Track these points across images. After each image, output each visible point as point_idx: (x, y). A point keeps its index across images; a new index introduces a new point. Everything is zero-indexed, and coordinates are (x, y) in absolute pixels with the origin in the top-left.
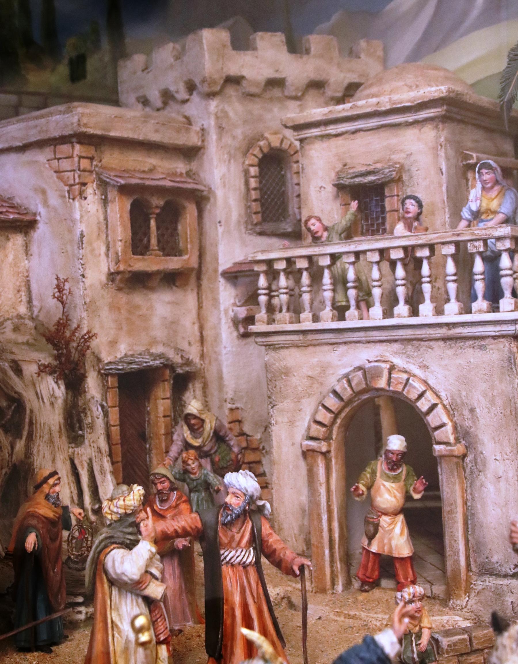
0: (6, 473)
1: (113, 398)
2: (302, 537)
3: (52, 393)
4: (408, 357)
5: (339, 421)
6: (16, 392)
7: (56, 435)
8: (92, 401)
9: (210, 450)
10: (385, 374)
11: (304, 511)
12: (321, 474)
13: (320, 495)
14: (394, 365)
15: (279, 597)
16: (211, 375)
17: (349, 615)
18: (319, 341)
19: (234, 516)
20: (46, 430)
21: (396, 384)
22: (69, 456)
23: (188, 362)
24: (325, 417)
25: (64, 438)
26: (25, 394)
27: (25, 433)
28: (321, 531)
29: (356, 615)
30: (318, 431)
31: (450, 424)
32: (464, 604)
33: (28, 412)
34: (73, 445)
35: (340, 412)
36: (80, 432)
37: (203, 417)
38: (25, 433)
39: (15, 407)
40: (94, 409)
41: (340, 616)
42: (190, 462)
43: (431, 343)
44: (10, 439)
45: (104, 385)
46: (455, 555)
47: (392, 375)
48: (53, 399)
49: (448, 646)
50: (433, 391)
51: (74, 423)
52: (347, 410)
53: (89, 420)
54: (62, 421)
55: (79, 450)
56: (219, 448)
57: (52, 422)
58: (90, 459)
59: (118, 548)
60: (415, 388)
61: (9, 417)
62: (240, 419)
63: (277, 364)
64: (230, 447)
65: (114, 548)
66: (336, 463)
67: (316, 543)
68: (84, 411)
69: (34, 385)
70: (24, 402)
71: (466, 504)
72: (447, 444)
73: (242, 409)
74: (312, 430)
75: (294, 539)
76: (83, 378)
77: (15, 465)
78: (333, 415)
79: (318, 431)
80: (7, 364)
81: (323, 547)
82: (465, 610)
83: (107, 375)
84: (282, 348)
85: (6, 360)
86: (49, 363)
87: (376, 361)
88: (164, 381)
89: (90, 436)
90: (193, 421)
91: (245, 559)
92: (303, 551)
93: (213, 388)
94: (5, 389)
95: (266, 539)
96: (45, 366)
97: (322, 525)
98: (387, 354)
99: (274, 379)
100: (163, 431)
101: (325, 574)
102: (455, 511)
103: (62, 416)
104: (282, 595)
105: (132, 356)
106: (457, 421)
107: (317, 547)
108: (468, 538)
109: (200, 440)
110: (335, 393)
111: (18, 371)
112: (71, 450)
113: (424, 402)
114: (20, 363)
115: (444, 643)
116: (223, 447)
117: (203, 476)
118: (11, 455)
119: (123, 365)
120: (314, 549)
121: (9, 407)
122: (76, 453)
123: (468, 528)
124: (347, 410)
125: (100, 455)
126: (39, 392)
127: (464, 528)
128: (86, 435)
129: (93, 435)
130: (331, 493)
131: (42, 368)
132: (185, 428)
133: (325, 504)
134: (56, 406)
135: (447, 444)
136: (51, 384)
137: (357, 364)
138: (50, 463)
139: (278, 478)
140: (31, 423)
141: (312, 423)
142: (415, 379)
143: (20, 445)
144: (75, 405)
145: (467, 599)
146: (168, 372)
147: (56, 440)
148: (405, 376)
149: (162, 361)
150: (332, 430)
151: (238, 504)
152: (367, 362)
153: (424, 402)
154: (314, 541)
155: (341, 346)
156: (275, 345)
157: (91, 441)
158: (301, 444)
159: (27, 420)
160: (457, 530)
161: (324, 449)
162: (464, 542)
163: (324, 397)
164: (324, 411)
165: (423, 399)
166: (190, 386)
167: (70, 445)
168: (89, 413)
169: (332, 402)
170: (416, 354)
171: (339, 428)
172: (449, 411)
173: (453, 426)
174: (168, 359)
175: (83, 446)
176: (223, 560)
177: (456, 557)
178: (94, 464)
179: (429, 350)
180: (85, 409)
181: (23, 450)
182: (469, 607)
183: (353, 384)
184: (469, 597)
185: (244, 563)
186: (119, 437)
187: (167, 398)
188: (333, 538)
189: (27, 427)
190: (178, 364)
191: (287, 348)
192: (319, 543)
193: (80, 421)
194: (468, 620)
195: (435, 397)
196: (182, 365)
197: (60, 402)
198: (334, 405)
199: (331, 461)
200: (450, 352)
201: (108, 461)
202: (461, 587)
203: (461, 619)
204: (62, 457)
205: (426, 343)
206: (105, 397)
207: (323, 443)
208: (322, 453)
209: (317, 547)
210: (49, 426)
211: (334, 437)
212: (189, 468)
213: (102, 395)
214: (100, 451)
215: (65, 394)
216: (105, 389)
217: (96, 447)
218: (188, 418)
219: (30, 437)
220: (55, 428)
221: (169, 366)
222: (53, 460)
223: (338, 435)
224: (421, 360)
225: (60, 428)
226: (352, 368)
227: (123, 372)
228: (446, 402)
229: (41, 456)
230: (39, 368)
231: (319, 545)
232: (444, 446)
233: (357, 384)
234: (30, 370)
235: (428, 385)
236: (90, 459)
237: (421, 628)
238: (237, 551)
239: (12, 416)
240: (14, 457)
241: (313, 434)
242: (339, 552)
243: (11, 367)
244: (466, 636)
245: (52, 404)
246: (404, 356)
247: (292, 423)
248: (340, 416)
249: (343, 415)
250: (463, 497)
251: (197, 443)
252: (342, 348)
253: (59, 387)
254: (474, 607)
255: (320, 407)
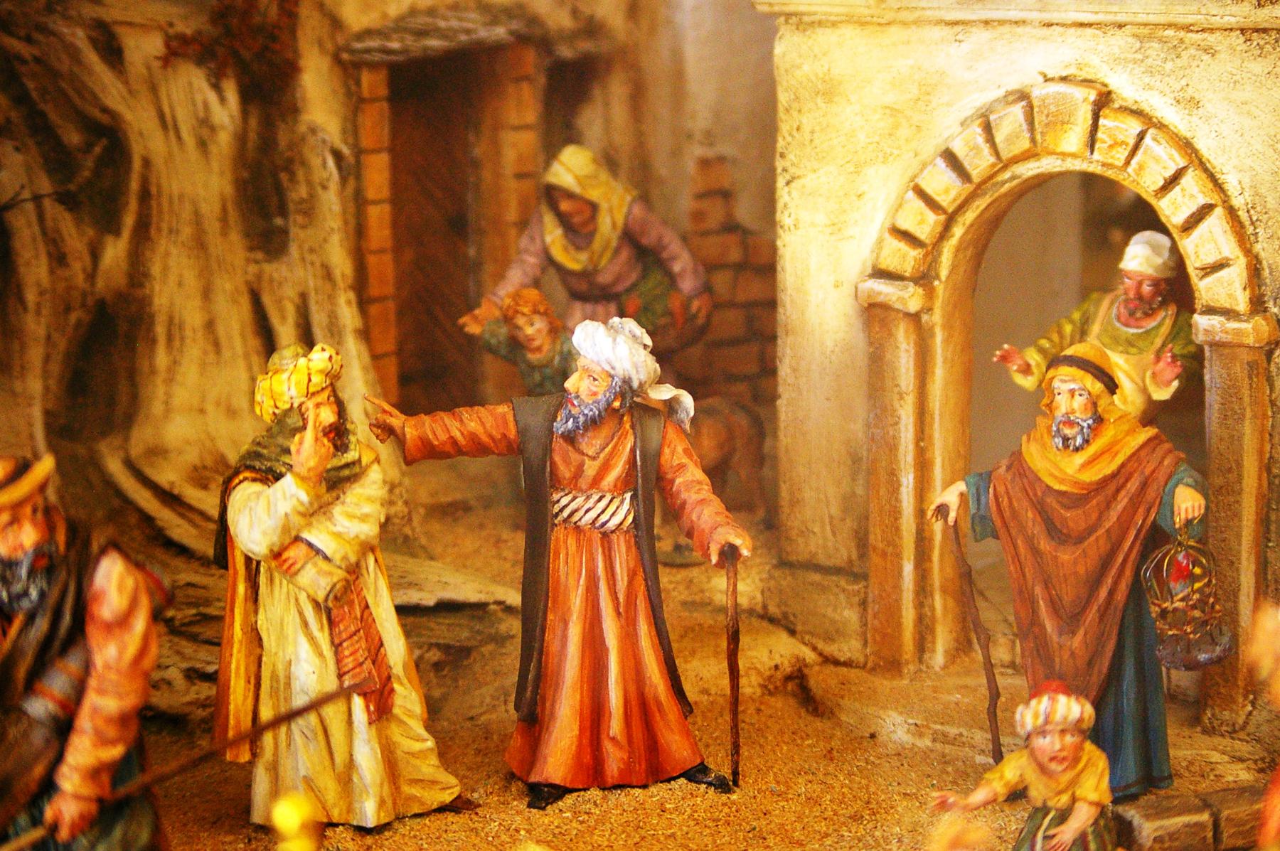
0: (79, 324)
1: (376, 125)
2: (850, 523)
3: (202, 114)
4: (1150, 71)
5: (958, 231)
6: (105, 110)
7: (213, 226)
8: (312, 140)
9: (618, 279)
10: (1084, 116)
11: (856, 460)
12: (903, 370)
13: (897, 423)
14: (1109, 93)
15: (779, 675)
16: (655, 63)
17: (945, 735)
18: (917, 14)
19: (582, 419)
20: (187, 213)
21: (1111, 147)
22: (248, 283)
23: (592, 28)
24: (922, 222)
25: (235, 237)
26: (128, 116)
27: (129, 220)
28: (896, 513)
29: (961, 735)
30: (903, 258)
31: (1242, 261)
32: (1241, 721)
33: (137, 164)
34: (259, 255)
35: (961, 208)
36: (279, 221)
37: (594, 194)
38: (129, 220)
39: (105, 149)
40: (315, 162)
41: (921, 735)
42: (521, 321)
43: (1211, 39)
44: (90, 232)
45: (349, 94)
46: (1228, 600)
47: (1101, 121)
48: (205, 132)
49: (1155, 839)
50: (1206, 170)
51: (265, 201)
52: (981, 203)
53: (303, 191)
54: (229, 190)
55: (275, 270)
56: (643, 277)
57: (202, 193)
58: (304, 296)
59: (254, 480)
60: (1157, 159)
61: (87, 174)
62: (726, 185)
63: (806, 68)
64: (672, 279)
65: (245, 479)
66: (946, 341)
67: (881, 545)
68: (289, 166)
69: (154, 89)
70: (127, 139)
71: (1269, 471)
72: (1229, 313)
73: (734, 161)
74: (886, 252)
75: (828, 528)
76: (288, 71)
77: (101, 304)
78: (942, 218)
79: (903, 258)
80: (80, 33)
81: (899, 556)
82: (1242, 735)
83: (358, 66)
84: (820, 23)
85: (80, 22)
86: (199, 32)
87: (1064, 79)
88: (518, 80)
89: (302, 234)
90: (565, 206)
91: (604, 518)
92: (850, 561)
93: (659, 96)
94: (77, 101)
95: (669, 476)
96: (184, 40)
97: (898, 500)
98: (1095, 61)
99: (795, 105)
100: (512, 214)
101: (899, 625)
102: (1237, 487)
103: (229, 176)
104: (789, 670)
105: (431, 12)
106: (1263, 255)
107: (884, 554)
108: (1266, 558)
109: (583, 257)
110: (951, 158)
111: (113, 53)
112: (253, 269)
113: (1180, 199)
114: (121, 31)
115: (1145, 833)
116: (656, 278)
117: (557, 359)
118: (91, 276)
119: (402, 40)
120: (875, 559)
121: (88, 147)
122: (266, 277)
123: (1268, 531)
124: (981, 203)
125: (328, 286)
126: (167, 110)
127: (1257, 531)
128: (294, 231)
129: (310, 232)
130: (928, 419)
131: (174, 44)
132: (549, 220)
133: (911, 447)
134: (213, 149)
135: (1229, 313)
136: (200, 90)
137: (1014, 84)
138: (197, 302)
139: (795, 370)
140: (145, 195)
141: (887, 235)
142: (1160, 136)
143: (115, 252)
144: (268, 143)
145: (1249, 708)
146: (530, 58)
147: (216, 244)
148: (1135, 126)
149: (515, 25)
150: (940, 255)
151: (595, 394)
152: (1041, 79)
153: (1180, 199)
154: (876, 537)
155: (974, 29)
156: (802, 14)
157: (306, 246)
158: (856, 288)
159: (134, 185)
160: (1239, 536)
161: (914, 305)
162: (1253, 567)
163: (924, 166)
164: (920, 204)
165: (1177, 189)
166: (597, 92)
167: (252, 255)
168: (300, 174)
169: (944, 185)
170: (1169, 66)
171: (958, 250)
172: (1242, 226)
173: (1249, 266)
174: (534, 20)
175: (285, 259)
176: (557, 515)
177: (1229, 605)
178: (314, 308)
179: (1206, 57)
180: (291, 161)
181: (124, 266)
182: (1251, 728)
183: (999, 138)
184: (1253, 703)
185: (604, 524)
186: (387, 232)
187: (527, 127)
188: (927, 534)
189: (133, 204)
190: (561, 30)
191: (834, 24)
192: (889, 544)
193: (280, 191)
194: (1241, 760)
195: (1211, 186)
196: (573, 36)
197: (224, 140)
198: (947, 191)
199: (933, 335)
200: (1258, 67)
201: (349, 303)
202: (1236, 679)
203: (1226, 758)
204: (228, 286)
205: (1200, 36)
206: (352, 128)
207: (912, 288)
208: (907, 315)
209: (884, 554)
210: (195, 204)
211: (944, 273)
212: (520, 335)
213: (345, 120)
214: (328, 274)
215: (238, 121)
216: (355, 104)
217: (318, 264)
218: (552, 194)
219: (143, 231)
220: (210, 209)
221: (534, 37)
222: (207, 293)
223: (954, 268)
224: (1184, 82)
225: (224, 209)
226: (1001, 93)
227: (400, 58)
228: (1237, 202)
229: (173, 278)
230: (167, 45)
231: (890, 550)
232: (1222, 319)
233: (1009, 140)
234: (143, 48)
235: (1195, 151)
236: (304, 296)
237: (1074, 800)
238: (588, 498)
239: (97, 172)
240: (100, 284)
241: (889, 263)
242: (942, 570)
243: (93, 42)
244: (1205, 817)
245: (203, 145)
246: (1138, 70)
247: (836, 228)
248: (960, 219)
249: (970, 216)
250: (1261, 452)
251: (574, 261)
252: (980, 36)
253: (222, 100)
254: (1265, 728)
255: (911, 194)
